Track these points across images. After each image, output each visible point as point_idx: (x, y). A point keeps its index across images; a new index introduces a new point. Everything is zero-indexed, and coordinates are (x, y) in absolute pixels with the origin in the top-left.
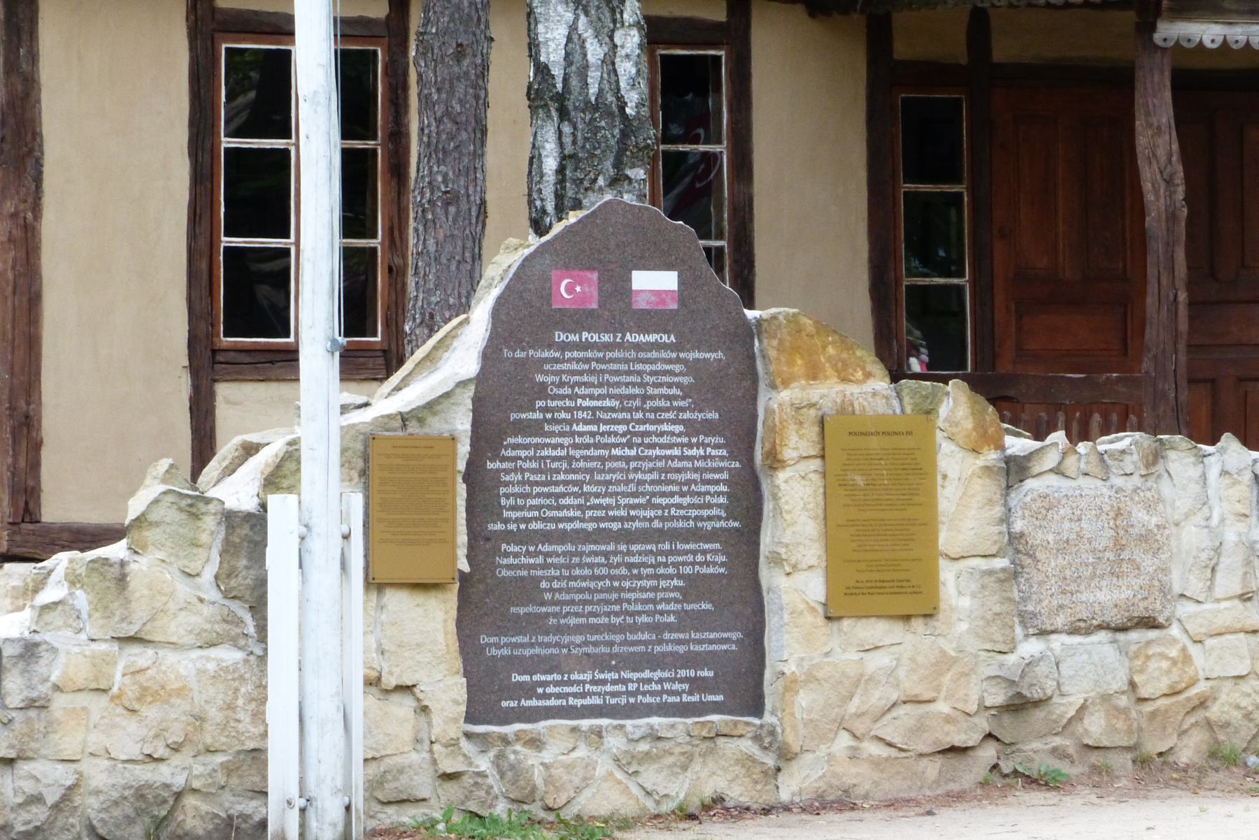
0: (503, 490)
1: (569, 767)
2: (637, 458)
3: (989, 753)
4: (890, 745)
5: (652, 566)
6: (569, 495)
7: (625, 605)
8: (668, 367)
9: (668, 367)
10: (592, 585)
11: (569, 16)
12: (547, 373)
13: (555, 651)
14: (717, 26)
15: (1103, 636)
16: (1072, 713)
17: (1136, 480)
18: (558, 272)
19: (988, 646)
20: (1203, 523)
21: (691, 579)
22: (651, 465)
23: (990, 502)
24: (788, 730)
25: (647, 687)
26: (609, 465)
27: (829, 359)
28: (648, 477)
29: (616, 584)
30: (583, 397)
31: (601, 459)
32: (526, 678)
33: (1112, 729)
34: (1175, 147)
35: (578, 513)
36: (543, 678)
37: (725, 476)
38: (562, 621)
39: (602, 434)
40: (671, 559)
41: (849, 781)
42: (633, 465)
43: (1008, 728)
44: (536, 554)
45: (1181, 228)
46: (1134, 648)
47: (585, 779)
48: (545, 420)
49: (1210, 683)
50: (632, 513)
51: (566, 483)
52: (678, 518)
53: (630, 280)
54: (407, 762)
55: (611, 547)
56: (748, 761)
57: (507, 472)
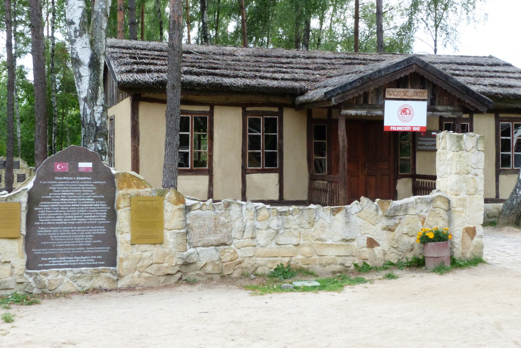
0: (39, 215)
1: (56, 280)
2: (80, 207)
3: (179, 275)
4: (150, 274)
5: (84, 232)
6: (59, 215)
7: (75, 241)
8: (89, 185)
9: (89, 185)
10: (66, 237)
11: (84, 103)
12: (53, 187)
13: (55, 252)
14: (276, 112)
15: (212, 247)
16: (202, 265)
17: (223, 211)
18: (56, 163)
19: (179, 250)
20: (241, 221)
21: (95, 235)
22: (84, 208)
23: (180, 216)
24: (120, 271)
25: (82, 261)
26: (71, 208)
27: (134, 183)
28: (83, 211)
29: (73, 236)
30: (64, 192)
31: (69, 207)
32: (46, 259)
33: (214, 269)
34: (345, 134)
35: (62, 220)
36: (51, 259)
37: (106, 211)
38: (57, 245)
39: (69, 201)
40: (89, 230)
41: (137, 283)
42: (78, 208)
43: (184, 269)
44: (49, 230)
45: (346, 149)
46: (221, 250)
47: (60, 283)
48: (52, 198)
49: (242, 258)
50: (78, 220)
51: (58, 213)
52: (91, 221)
53: (78, 165)
54: (7, 280)
55: (72, 228)
56: (109, 278)
57: (41, 210)
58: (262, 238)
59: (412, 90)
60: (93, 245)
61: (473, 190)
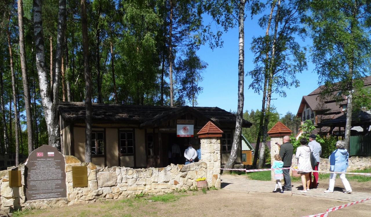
43: (96, 197)
58: (130, 182)
59: (188, 120)
60: (56, 188)
61: (216, 159)
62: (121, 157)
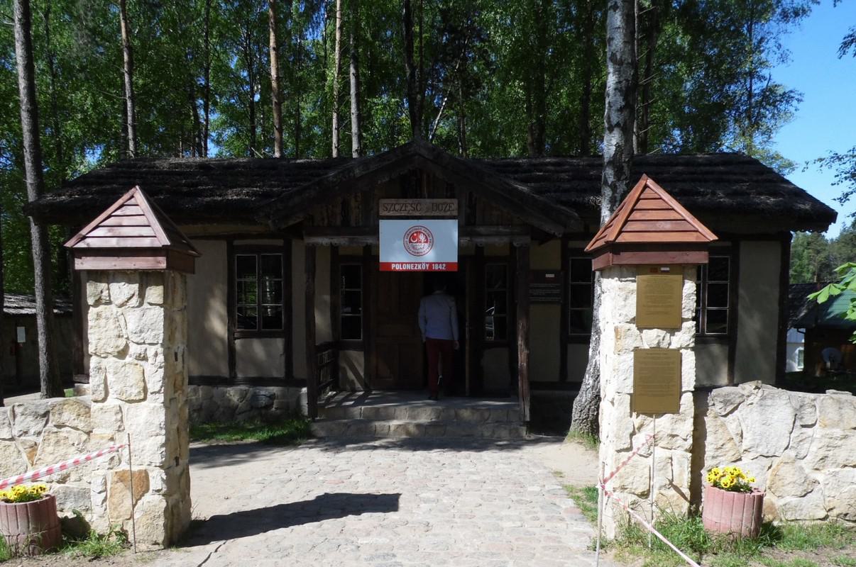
53: (21, 326)
59: (428, 201)
62: (238, 342)
